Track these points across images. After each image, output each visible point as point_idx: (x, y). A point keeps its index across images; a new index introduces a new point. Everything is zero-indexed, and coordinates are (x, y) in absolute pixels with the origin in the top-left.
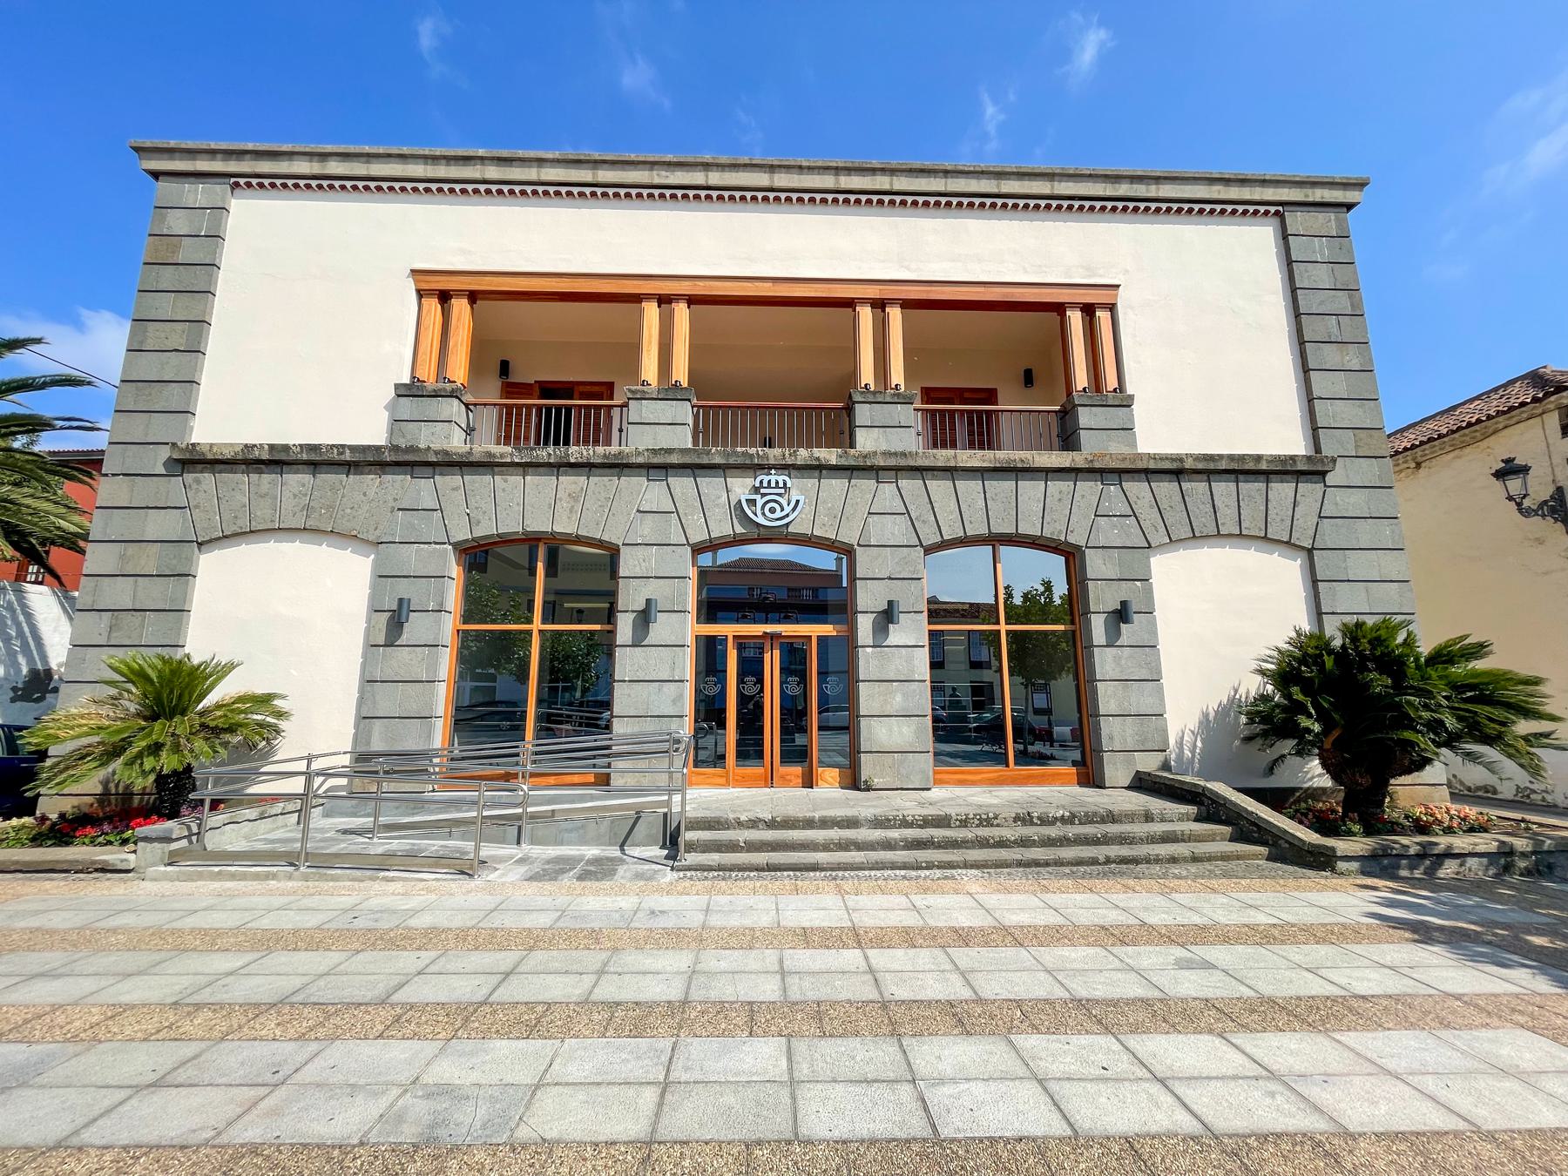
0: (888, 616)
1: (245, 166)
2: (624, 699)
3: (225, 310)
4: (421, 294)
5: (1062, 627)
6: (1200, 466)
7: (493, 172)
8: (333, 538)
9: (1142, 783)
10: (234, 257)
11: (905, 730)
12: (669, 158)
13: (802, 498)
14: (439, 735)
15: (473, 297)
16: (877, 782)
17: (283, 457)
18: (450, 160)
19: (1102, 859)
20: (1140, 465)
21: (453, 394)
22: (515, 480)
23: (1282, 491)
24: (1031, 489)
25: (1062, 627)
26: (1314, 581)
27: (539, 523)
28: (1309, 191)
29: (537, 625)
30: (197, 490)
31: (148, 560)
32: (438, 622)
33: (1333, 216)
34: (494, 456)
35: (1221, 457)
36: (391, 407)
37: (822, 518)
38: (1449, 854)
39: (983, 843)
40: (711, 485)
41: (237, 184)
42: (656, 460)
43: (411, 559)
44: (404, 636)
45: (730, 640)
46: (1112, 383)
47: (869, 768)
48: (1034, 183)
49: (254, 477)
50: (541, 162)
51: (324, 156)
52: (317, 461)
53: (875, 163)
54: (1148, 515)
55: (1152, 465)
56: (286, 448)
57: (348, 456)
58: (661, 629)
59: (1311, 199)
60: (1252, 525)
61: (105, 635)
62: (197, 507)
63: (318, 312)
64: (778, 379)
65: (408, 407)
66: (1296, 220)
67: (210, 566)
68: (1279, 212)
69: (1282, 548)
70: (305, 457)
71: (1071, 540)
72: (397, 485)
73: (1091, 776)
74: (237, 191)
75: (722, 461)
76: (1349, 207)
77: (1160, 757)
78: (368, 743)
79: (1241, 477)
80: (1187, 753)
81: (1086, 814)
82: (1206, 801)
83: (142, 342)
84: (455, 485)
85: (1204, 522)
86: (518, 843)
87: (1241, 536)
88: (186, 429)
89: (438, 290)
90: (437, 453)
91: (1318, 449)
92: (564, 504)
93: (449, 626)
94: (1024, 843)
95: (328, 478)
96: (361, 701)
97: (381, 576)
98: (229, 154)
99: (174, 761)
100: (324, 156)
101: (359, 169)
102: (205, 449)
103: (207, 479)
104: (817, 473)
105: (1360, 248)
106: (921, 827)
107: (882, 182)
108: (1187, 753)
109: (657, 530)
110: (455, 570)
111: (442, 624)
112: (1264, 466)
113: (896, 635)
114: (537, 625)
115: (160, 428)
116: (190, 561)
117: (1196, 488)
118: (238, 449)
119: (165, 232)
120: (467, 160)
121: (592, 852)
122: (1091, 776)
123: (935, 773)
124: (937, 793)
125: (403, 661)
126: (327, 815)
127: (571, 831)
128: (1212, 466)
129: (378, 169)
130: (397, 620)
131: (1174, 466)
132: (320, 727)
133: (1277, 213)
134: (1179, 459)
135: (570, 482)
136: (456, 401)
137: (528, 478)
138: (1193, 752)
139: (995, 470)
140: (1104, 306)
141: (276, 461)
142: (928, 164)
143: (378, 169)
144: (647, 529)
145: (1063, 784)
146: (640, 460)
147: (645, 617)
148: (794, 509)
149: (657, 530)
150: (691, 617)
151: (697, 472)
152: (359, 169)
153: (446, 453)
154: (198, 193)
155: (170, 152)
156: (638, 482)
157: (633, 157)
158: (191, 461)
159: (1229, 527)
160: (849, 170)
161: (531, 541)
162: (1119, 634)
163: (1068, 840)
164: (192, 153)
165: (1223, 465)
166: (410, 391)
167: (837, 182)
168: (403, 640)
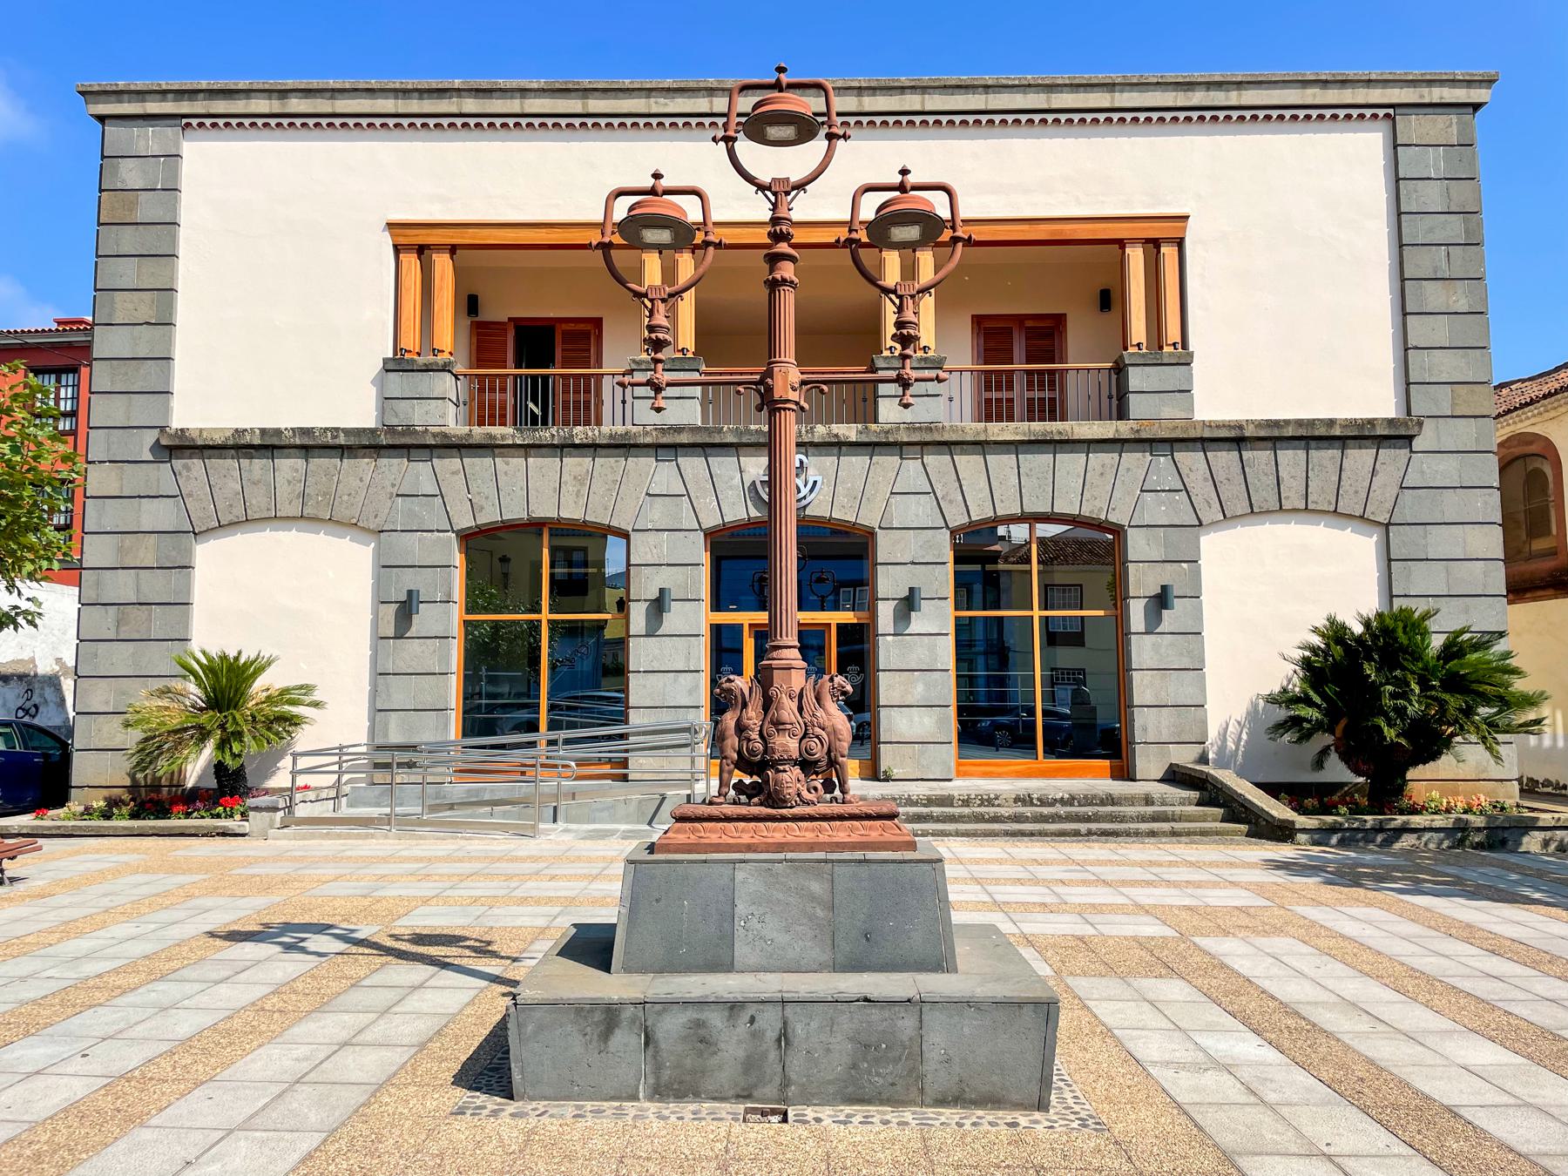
0: (909, 603)
1: (199, 107)
2: (639, 690)
3: (189, 273)
4: (398, 249)
5: (1101, 613)
6: (1262, 433)
7: (470, 105)
8: (330, 526)
9: (1176, 776)
10: (193, 210)
11: (926, 720)
12: (668, 82)
13: (819, 479)
14: (453, 730)
15: (453, 249)
16: (897, 772)
17: (275, 441)
18: (423, 93)
19: (1083, 831)
20: (1193, 434)
21: (446, 368)
22: (517, 462)
23: (1360, 458)
24: (1071, 462)
25: (1101, 613)
26: (1388, 560)
27: (544, 509)
28: (1425, 91)
29: (545, 616)
30: (188, 478)
31: (146, 552)
32: (448, 613)
33: (1454, 118)
34: (495, 438)
35: (1287, 422)
36: (379, 382)
37: (841, 499)
38: (1405, 829)
39: (980, 818)
40: (724, 465)
41: (188, 125)
42: (664, 440)
43: (414, 547)
44: (413, 629)
45: (746, 628)
46: (1173, 334)
47: (889, 758)
48: (1091, 95)
49: (245, 462)
50: (524, 92)
51: (283, 93)
52: (310, 445)
53: (904, 80)
54: (1201, 488)
55: (1207, 434)
56: (278, 432)
57: (342, 440)
58: (674, 619)
59: (1426, 100)
60: (1321, 497)
61: (113, 629)
62: (190, 495)
63: (286, 272)
64: (793, 323)
65: (398, 384)
66: (1411, 127)
67: (208, 556)
68: (1392, 113)
69: (1356, 523)
70: (298, 442)
71: (1112, 518)
72: (394, 469)
73: (1125, 773)
74: (188, 132)
75: (735, 440)
76: (1476, 107)
77: (1198, 749)
78: (386, 735)
79: (1313, 444)
80: (1231, 745)
81: (1086, 797)
82: (1210, 787)
83: (110, 315)
84: (454, 468)
85: (1264, 495)
86: (555, 821)
87: (1307, 511)
88: (167, 411)
89: (414, 243)
90: (434, 435)
91: (1409, 414)
92: (569, 488)
93: (454, 617)
94: (1017, 818)
95: (319, 463)
96: (374, 693)
97: (384, 567)
98: (180, 94)
99: (215, 756)
100: (283, 93)
101: (323, 105)
102: (195, 435)
103: (197, 464)
104: (835, 450)
105: (1484, 160)
106: (925, 806)
107: (912, 102)
108: (1231, 745)
109: (662, 518)
110: (458, 559)
111: (447, 618)
112: (1337, 432)
113: (918, 623)
114: (545, 616)
115: (141, 410)
116: (189, 552)
117: (1259, 458)
118: (229, 434)
119: (119, 186)
120: (441, 92)
121: (623, 827)
122: (1125, 773)
123: (959, 765)
124: (957, 783)
125: (411, 653)
126: (350, 805)
127: (602, 810)
128: (1276, 433)
129: (343, 105)
130: (406, 609)
131: (1232, 434)
132: (339, 721)
133: (1387, 116)
134: (1239, 426)
135: (575, 464)
136: (448, 375)
137: (530, 460)
138: (1237, 745)
139: (1030, 442)
140: (1169, 240)
141: (269, 446)
142: (965, 78)
143: (343, 105)
144: (657, 514)
145: (1095, 777)
146: (648, 440)
147: (659, 606)
148: (811, 491)
149: (662, 518)
150: (705, 605)
151: (709, 451)
152: (323, 105)
153: (445, 435)
154: (150, 139)
155: (118, 94)
156: (646, 463)
157: (627, 83)
158: (178, 447)
159: (1293, 499)
160: (873, 90)
161: (535, 526)
162: (1159, 620)
163: (1060, 817)
164: (141, 95)
165: (1289, 432)
166: (398, 364)
167: (860, 103)
168: (412, 632)
